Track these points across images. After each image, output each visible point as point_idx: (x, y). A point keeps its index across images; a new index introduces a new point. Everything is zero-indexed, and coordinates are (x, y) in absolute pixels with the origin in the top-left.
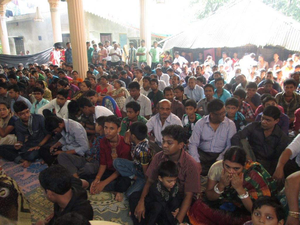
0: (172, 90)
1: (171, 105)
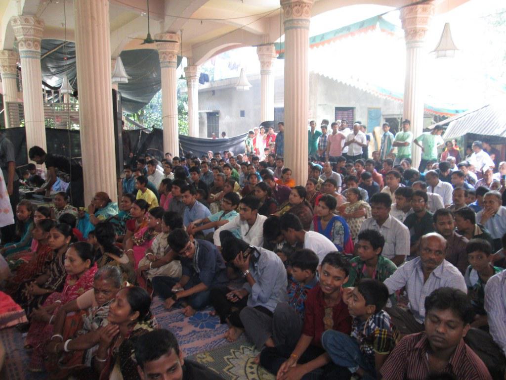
0: (450, 216)
1: (445, 245)
